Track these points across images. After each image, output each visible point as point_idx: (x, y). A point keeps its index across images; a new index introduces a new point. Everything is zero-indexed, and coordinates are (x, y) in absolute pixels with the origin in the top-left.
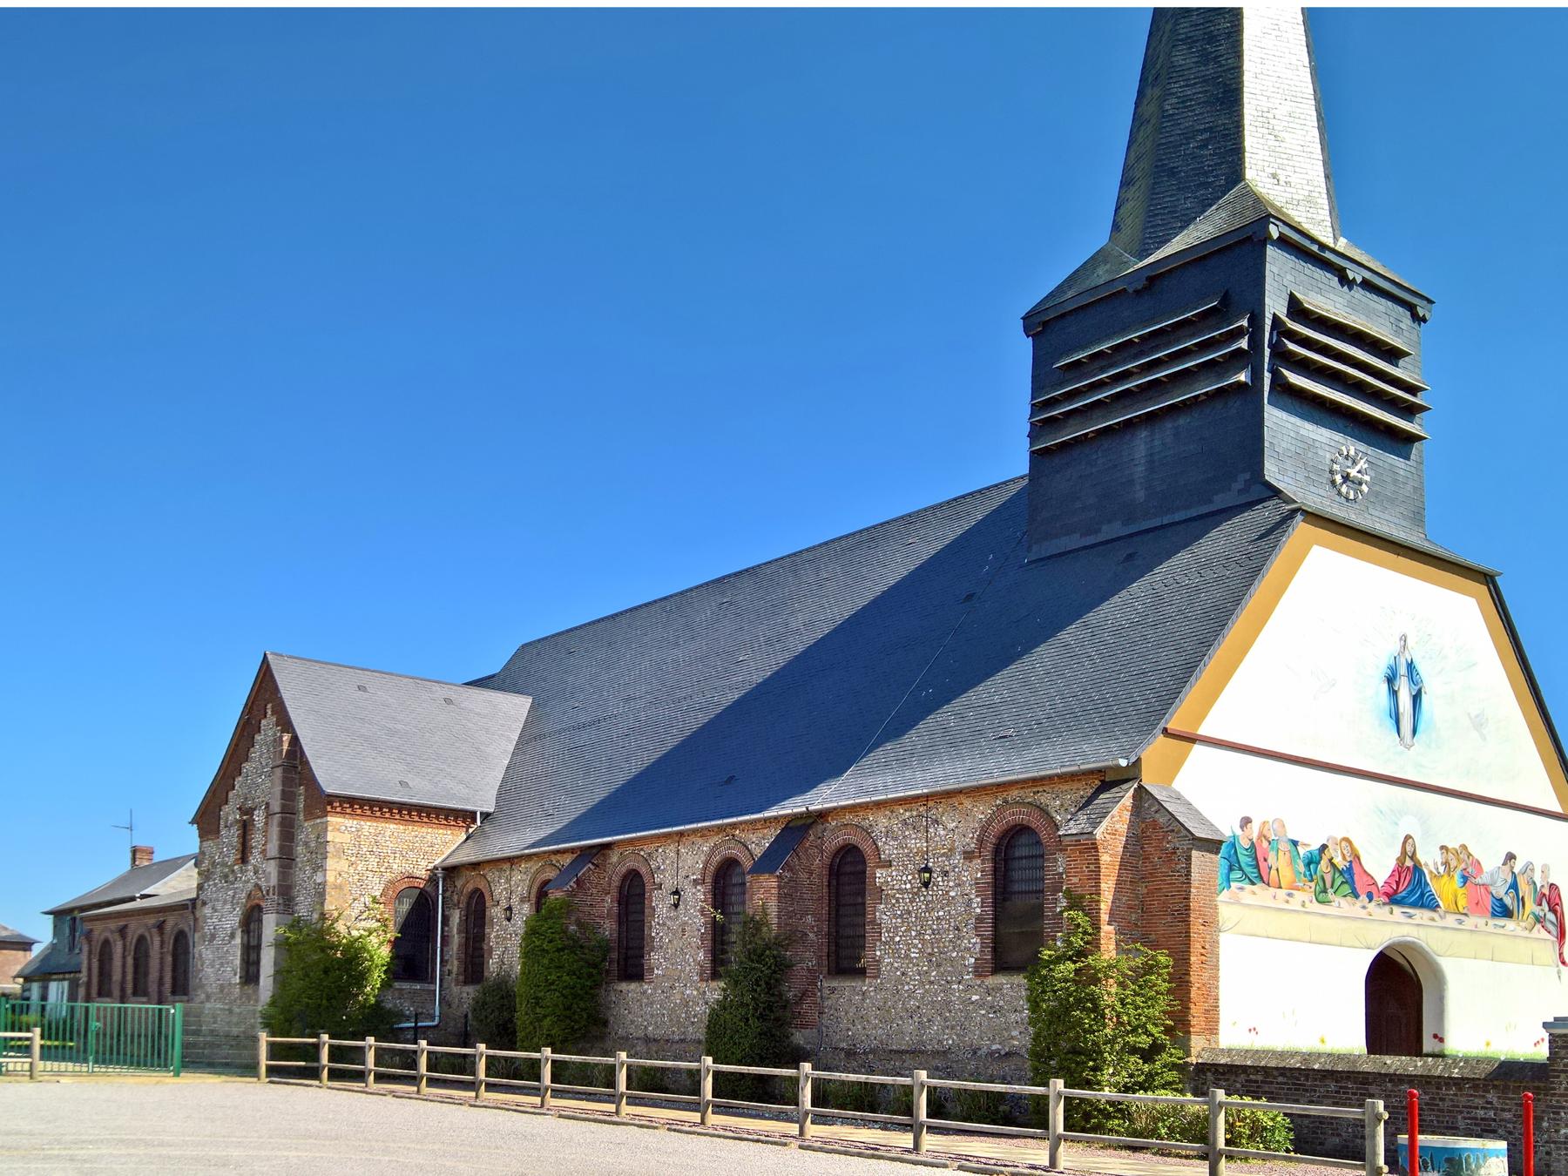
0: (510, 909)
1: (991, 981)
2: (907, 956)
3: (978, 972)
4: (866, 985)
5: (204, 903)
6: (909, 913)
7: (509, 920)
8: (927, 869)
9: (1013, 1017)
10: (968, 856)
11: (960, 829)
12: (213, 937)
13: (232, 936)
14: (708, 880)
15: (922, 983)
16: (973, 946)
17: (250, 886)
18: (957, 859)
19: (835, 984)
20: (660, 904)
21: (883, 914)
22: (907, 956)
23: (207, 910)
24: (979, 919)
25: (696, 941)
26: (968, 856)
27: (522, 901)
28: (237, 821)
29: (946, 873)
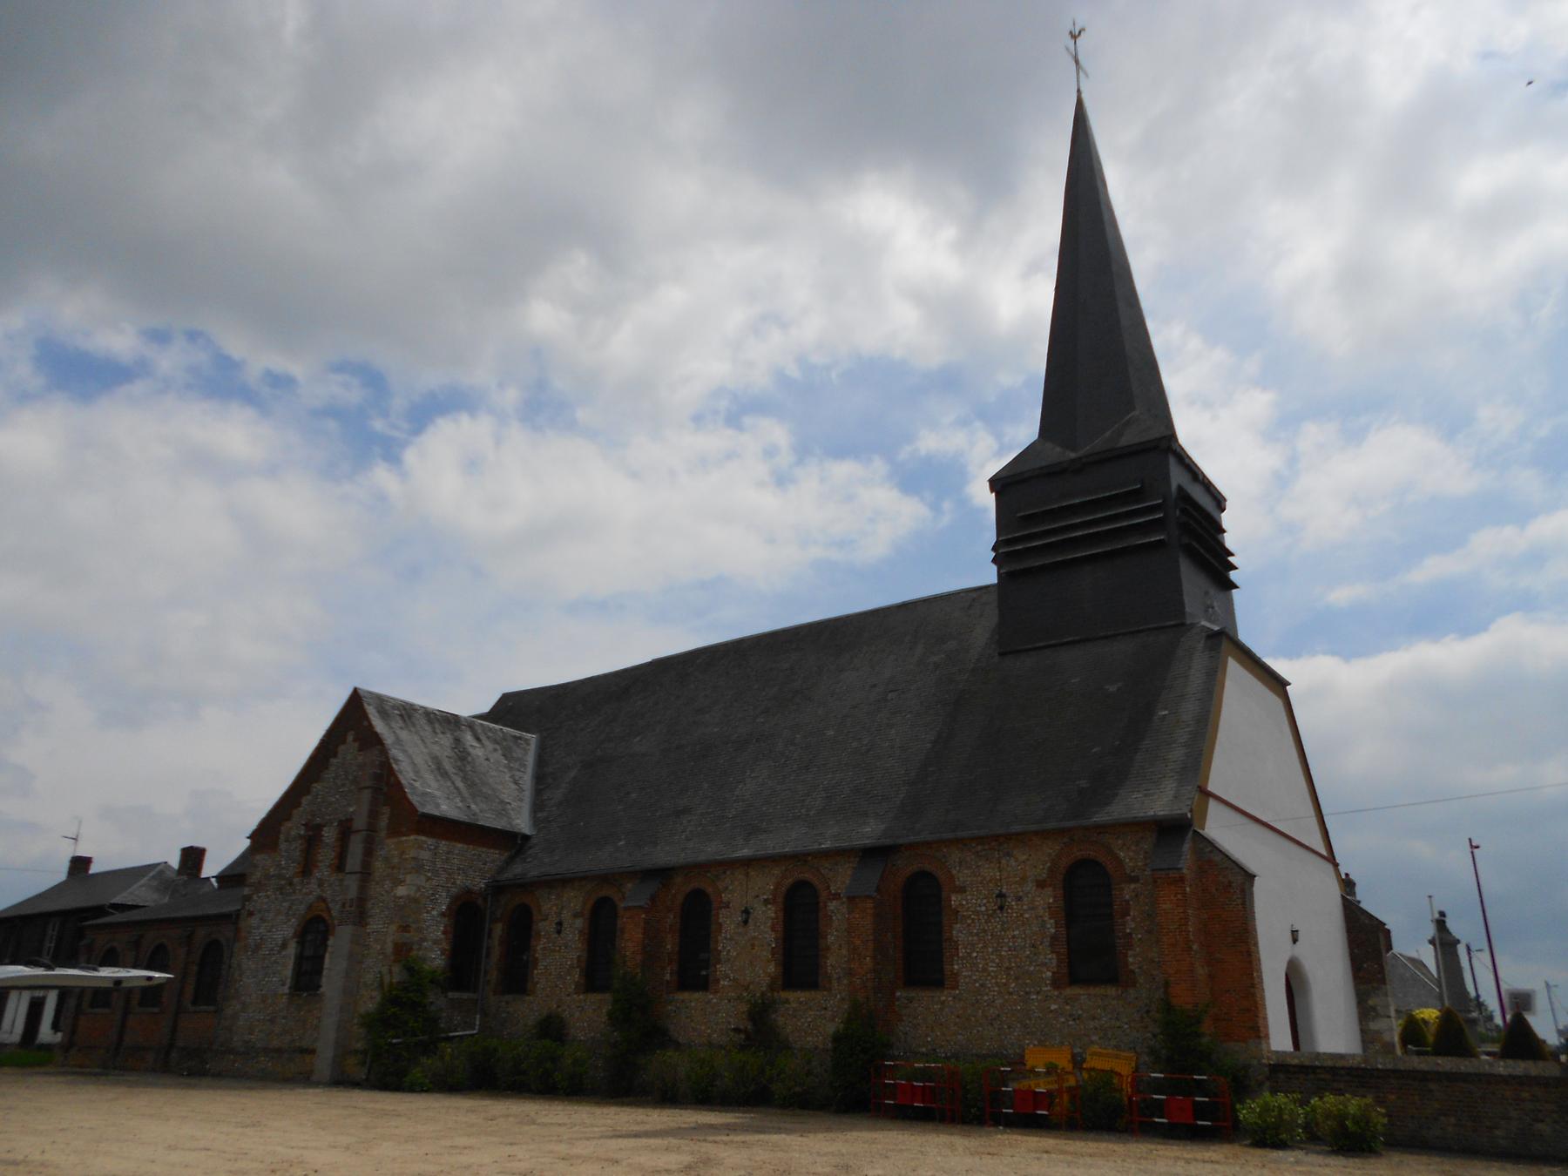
0: (560, 924)
1: (1069, 991)
2: (985, 970)
3: (1056, 983)
4: (944, 996)
5: (251, 914)
6: (985, 931)
7: (559, 932)
8: (1001, 895)
9: (1092, 1024)
10: (766, 902)
11: (765, 884)
12: (258, 947)
13: (284, 946)
14: (780, 900)
15: (1000, 992)
16: (1048, 962)
17: (311, 898)
18: (1030, 886)
19: (912, 994)
20: (728, 922)
21: (959, 932)
22: (985, 970)
23: (254, 921)
24: (1054, 938)
25: (767, 954)
26: (1041, 884)
27: (576, 916)
28: (301, 837)
29: (1019, 899)
